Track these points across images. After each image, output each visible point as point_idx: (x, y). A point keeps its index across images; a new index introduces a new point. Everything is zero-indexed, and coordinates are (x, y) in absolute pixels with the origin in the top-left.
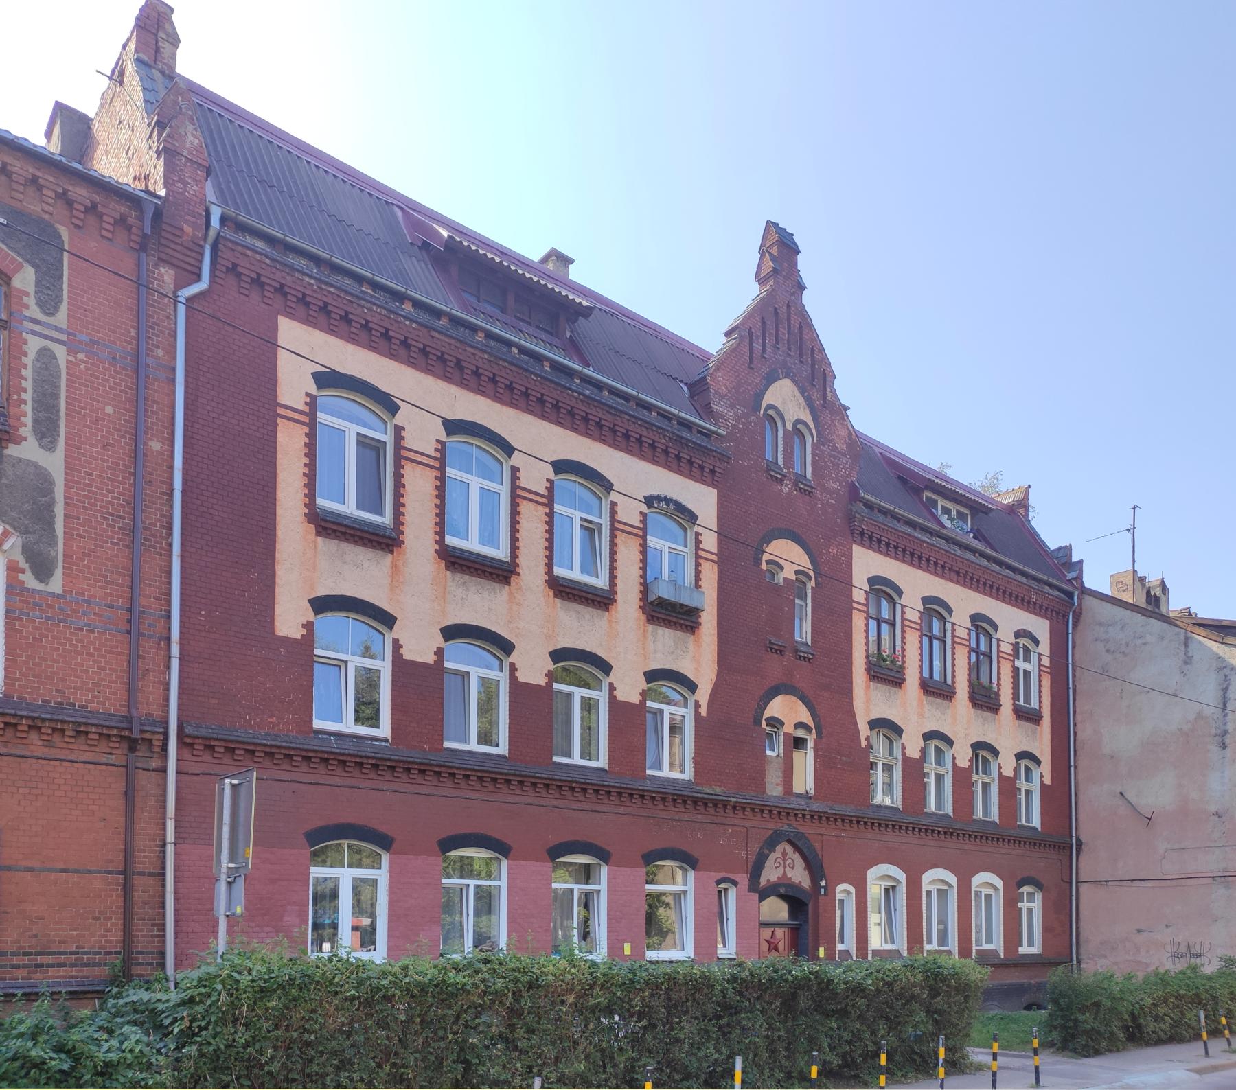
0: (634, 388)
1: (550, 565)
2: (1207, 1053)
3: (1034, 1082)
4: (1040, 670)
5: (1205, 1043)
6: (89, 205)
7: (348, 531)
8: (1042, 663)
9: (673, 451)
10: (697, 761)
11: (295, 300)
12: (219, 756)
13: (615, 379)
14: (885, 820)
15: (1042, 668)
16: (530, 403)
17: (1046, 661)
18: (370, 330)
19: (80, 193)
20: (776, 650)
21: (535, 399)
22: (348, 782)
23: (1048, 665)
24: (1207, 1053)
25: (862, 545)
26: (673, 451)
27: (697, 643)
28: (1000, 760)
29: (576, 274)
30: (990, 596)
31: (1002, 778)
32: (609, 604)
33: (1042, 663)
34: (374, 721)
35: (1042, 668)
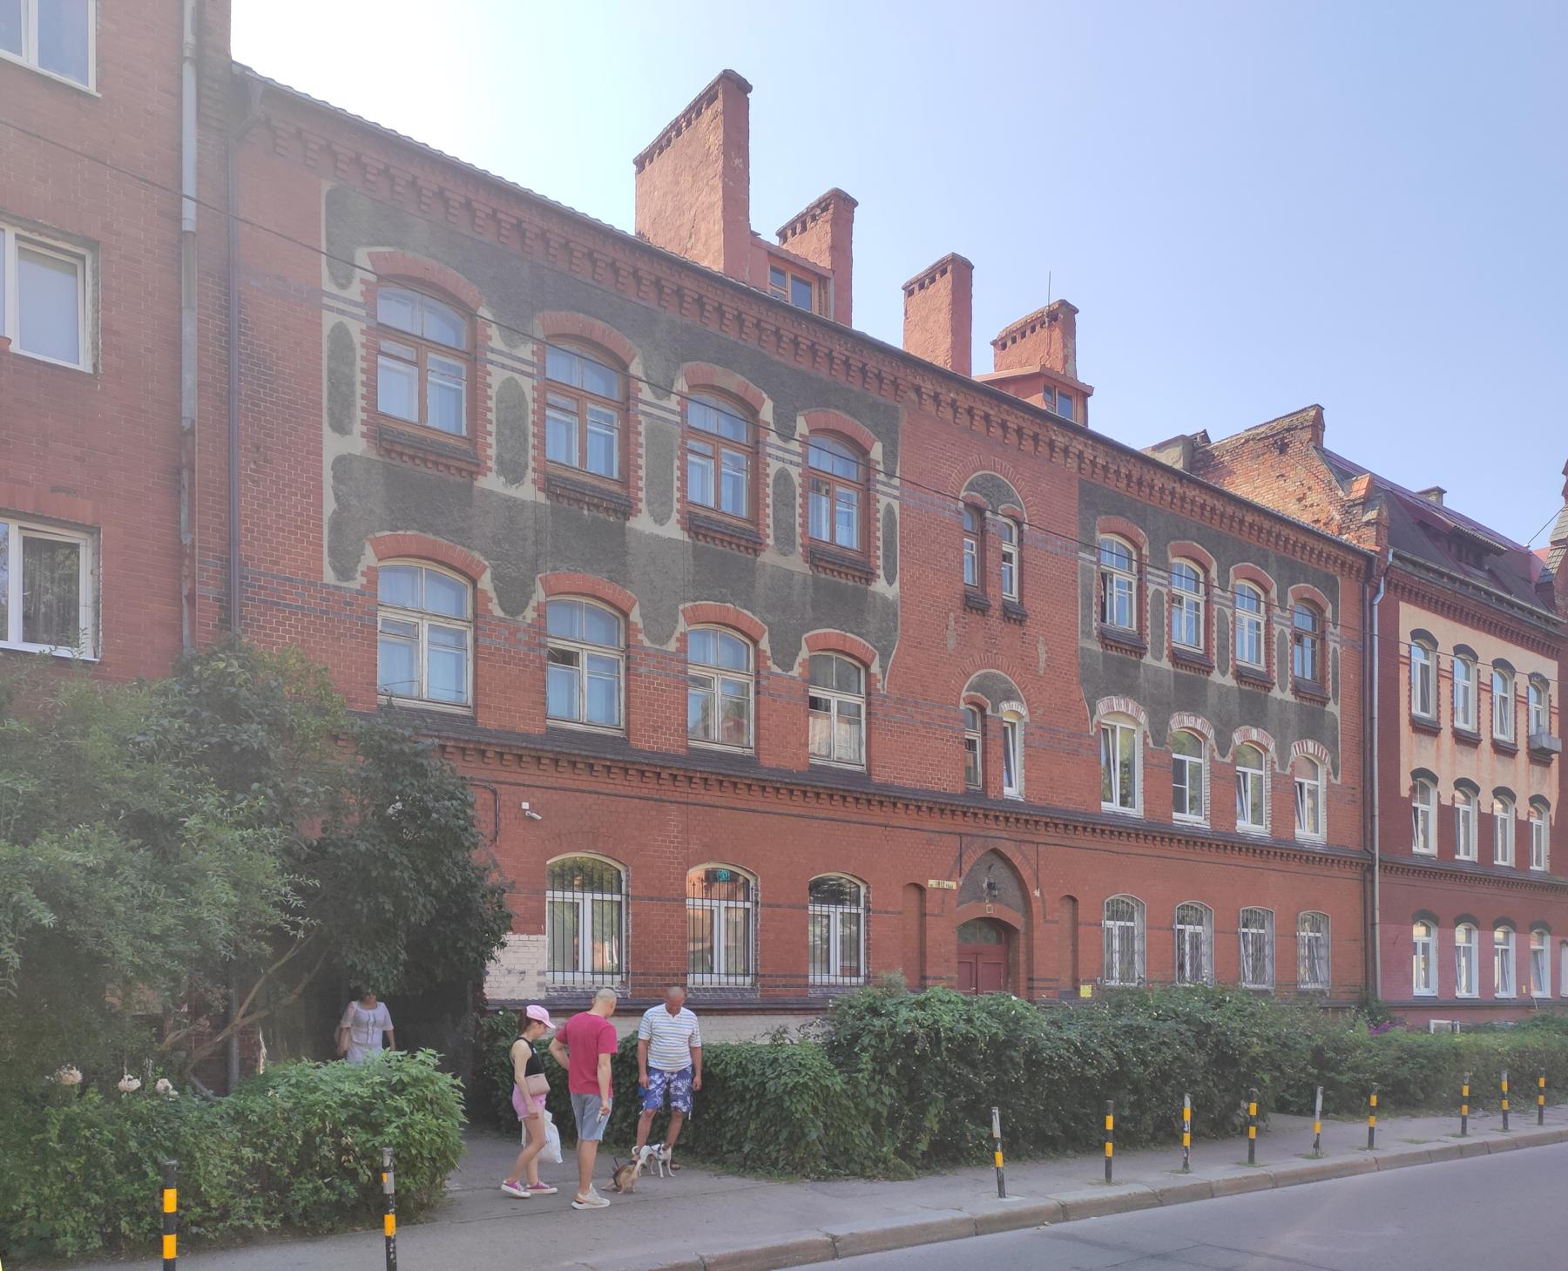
0: (1436, 563)
1: (1452, 721)
2: (1108, 1175)
3: (1103, 1176)
4: (1479, 689)
5: (1108, 1162)
6: (437, 190)
7: (407, 451)
8: (1552, 704)
9: (1012, 426)
10: (1551, 858)
11: (509, 227)
12: (545, 767)
13: (1523, 600)
14: (1102, 824)
15: (1482, 686)
16: (451, 210)
17: (1555, 703)
18: (499, 222)
19: (840, 350)
20: (1015, 620)
21: (690, 300)
22: (610, 789)
23: (1557, 706)
24: (1108, 1175)
25: (1408, 602)
26: (786, 333)
27: (1550, 773)
28: (1479, 797)
29: (1449, 502)
30: (1429, 609)
31: (1441, 807)
32: (478, 473)
33: (1442, 666)
34: (65, 630)
35: (1482, 686)
